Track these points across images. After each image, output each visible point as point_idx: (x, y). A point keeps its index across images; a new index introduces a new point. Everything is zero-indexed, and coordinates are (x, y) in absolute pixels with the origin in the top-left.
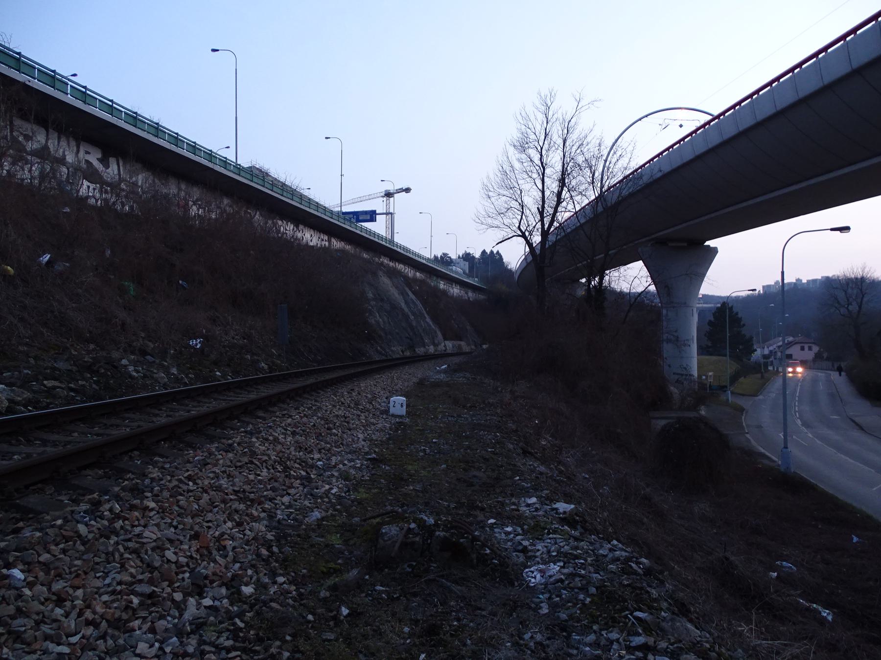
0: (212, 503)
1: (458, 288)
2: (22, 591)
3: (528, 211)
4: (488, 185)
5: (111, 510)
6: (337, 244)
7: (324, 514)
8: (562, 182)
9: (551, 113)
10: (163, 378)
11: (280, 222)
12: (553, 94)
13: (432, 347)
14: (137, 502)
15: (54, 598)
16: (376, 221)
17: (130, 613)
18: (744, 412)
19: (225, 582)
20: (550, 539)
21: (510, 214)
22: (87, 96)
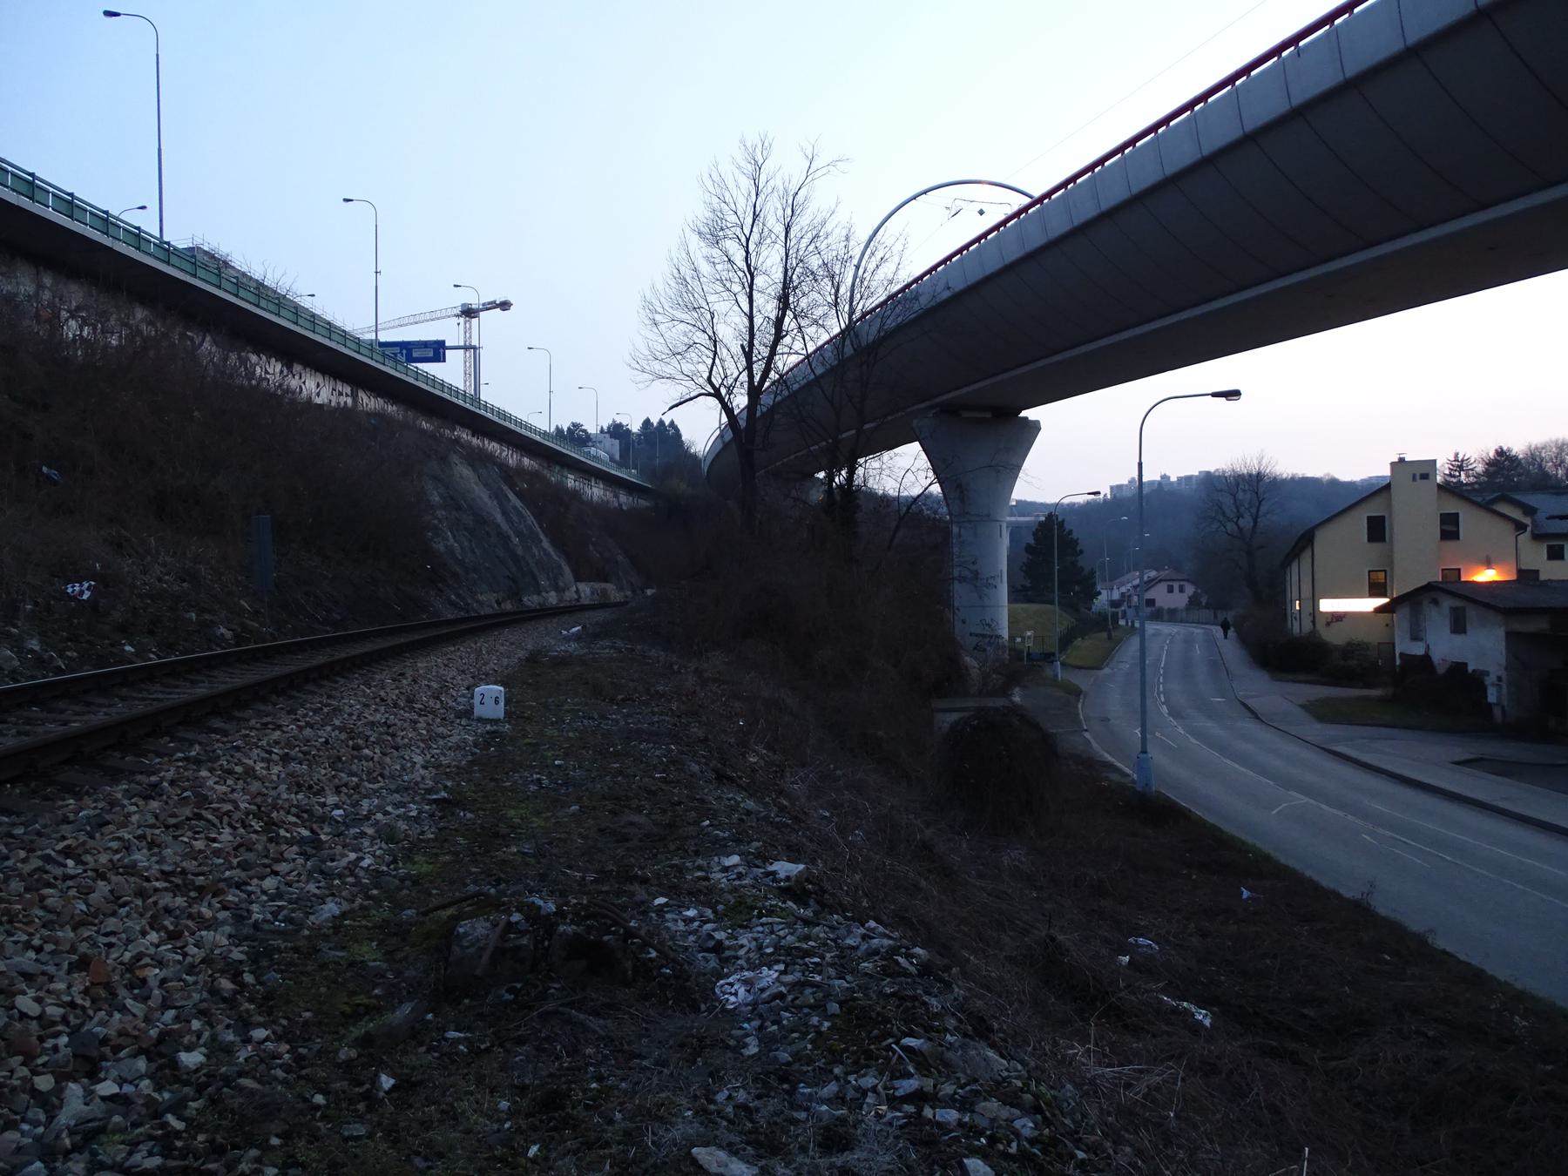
0: (116, 898)
1: (601, 486)
3: (725, 351)
6: (369, 402)
7: (346, 906)
8: (784, 301)
12: (766, 144)
13: (553, 593)
16: (444, 361)
18: (1082, 697)
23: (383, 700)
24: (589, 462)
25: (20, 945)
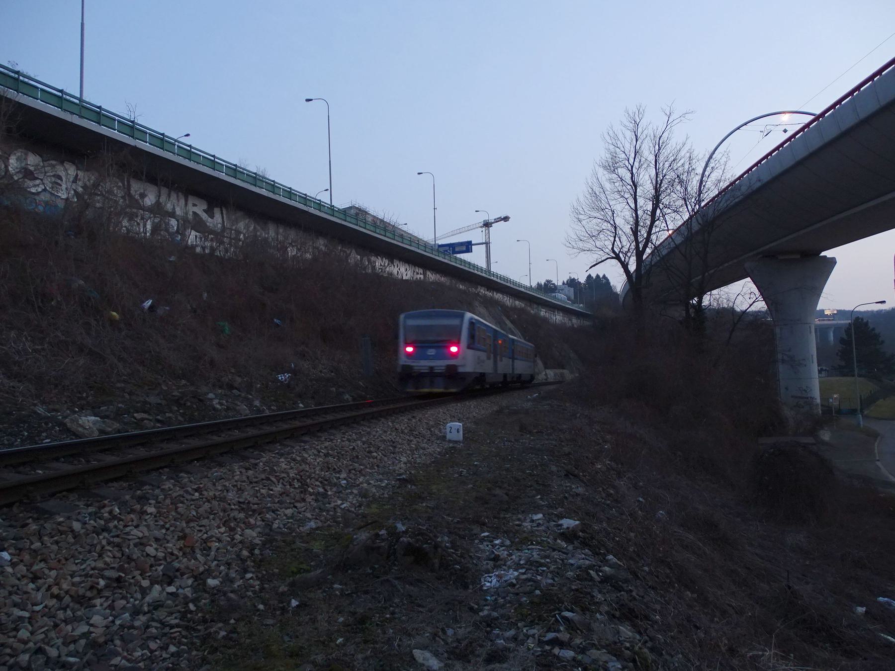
0: (211, 512)
1: (561, 315)
2: (4, 569)
3: (620, 232)
4: (578, 208)
5: (110, 512)
6: (432, 277)
7: (320, 524)
8: (656, 200)
9: (640, 130)
10: (245, 410)
11: (373, 258)
12: (641, 110)
14: (138, 507)
15: (31, 576)
16: (472, 252)
17: (95, 592)
18: (879, 438)
19: (195, 574)
20: (528, 549)
21: (601, 236)
23: (396, 429)
24: (553, 301)
25: (159, 526)
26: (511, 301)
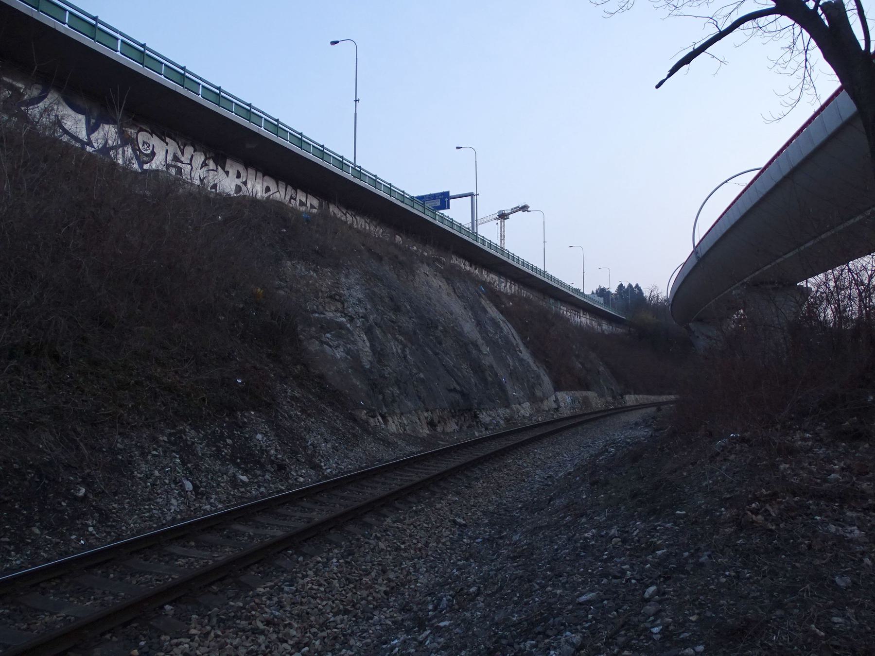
1: (588, 317)
13: (527, 405)
16: (449, 208)
22: (362, 174)
26: (513, 288)
